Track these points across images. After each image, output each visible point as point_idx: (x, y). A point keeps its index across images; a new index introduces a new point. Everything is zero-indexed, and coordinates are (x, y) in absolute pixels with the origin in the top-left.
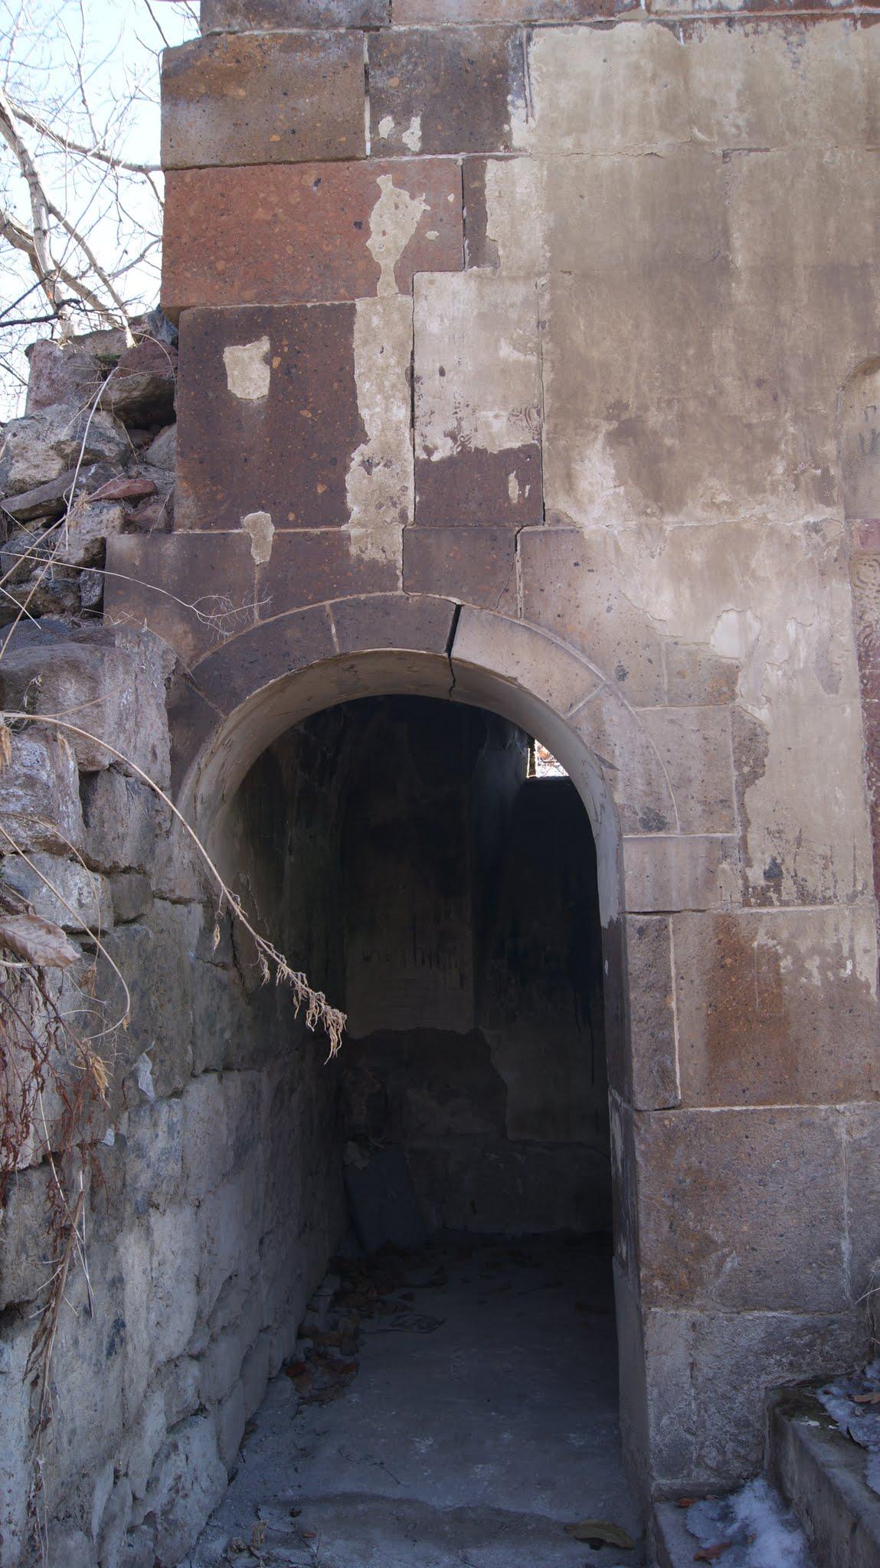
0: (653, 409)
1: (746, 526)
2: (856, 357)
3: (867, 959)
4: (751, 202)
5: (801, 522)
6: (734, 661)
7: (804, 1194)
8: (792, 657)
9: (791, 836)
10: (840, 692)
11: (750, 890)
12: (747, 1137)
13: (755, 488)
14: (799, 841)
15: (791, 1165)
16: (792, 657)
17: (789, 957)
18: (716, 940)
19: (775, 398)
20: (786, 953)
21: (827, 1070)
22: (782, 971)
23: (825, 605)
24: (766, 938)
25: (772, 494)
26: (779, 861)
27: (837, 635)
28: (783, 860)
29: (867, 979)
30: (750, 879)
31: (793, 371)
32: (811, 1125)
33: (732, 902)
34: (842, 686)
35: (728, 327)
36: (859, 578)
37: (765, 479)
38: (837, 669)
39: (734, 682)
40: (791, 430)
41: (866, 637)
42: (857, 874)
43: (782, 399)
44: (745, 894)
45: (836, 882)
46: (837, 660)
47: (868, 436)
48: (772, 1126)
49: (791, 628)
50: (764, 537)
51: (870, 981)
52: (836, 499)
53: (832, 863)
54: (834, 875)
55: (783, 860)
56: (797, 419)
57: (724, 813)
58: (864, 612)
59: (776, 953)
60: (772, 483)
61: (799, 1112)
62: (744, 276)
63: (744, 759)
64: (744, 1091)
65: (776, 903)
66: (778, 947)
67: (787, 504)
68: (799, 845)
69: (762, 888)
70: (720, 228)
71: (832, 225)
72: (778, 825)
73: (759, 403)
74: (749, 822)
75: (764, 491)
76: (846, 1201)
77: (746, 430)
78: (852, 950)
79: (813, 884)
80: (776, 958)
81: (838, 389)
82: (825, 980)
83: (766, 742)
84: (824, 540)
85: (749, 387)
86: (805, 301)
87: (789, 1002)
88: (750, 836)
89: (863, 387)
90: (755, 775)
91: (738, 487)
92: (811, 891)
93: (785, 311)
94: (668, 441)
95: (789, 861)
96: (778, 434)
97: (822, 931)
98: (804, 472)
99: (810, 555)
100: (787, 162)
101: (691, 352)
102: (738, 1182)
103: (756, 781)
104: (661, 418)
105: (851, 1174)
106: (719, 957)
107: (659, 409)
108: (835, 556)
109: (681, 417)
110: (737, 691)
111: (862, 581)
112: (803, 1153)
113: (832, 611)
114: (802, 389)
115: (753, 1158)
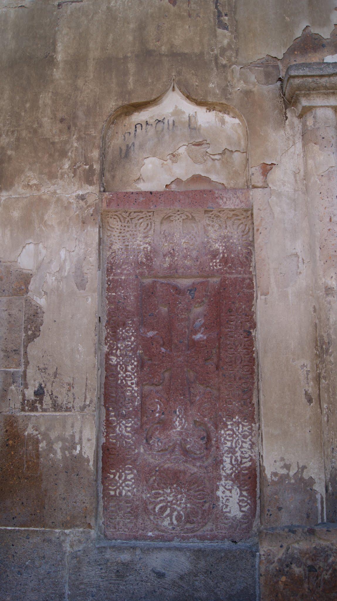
0: (4, 136)
1: (44, 197)
2: (115, 105)
3: (89, 444)
4: (70, 28)
5: (74, 194)
6: (30, 272)
7: (43, 581)
8: (61, 269)
9: (51, 371)
10: (87, 289)
11: (26, 402)
12: (13, 545)
13: (52, 176)
14: (55, 375)
15: (37, 563)
16: (61, 269)
17: (44, 442)
18: (5, 430)
19: (69, 128)
20: (43, 439)
21: (61, 509)
22: (40, 449)
23: (83, 240)
24: (32, 430)
25: (61, 179)
26: (43, 386)
27: (88, 257)
28: (45, 385)
29: (88, 456)
30: (26, 395)
31: (80, 114)
32: (50, 541)
33: (15, 408)
34: (88, 286)
35: (49, 92)
36: (109, 226)
37: (58, 172)
38: (86, 276)
39: (29, 284)
40: (75, 145)
41: (112, 258)
42: (87, 395)
43: (73, 128)
44: (23, 404)
45: (74, 398)
46: (85, 271)
47: (124, 148)
48: (27, 540)
49: (63, 253)
50: (53, 203)
51: (90, 457)
52: (95, 182)
53: (73, 387)
54: (73, 394)
55: (45, 385)
56: (79, 139)
57: (15, 357)
58: (112, 244)
59: (38, 439)
60: (62, 174)
61: (43, 533)
62: (61, 65)
63: (29, 327)
64: (13, 518)
65: (39, 410)
66: (39, 436)
67: (68, 185)
68: (55, 377)
69: (32, 401)
70: (51, 41)
71: (111, 36)
72: (44, 365)
73: (61, 131)
74: (28, 362)
75: (57, 178)
76: (67, 587)
77: (51, 146)
78: (81, 439)
79: (61, 400)
80: (38, 442)
81: (104, 122)
82: (64, 456)
83: (43, 317)
84: (86, 204)
85: (56, 123)
86: (92, 77)
87: (43, 468)
88: (28, 371)
89: (124, 123)
90: (35, 336)
91: (43, 176)
92: (60, 404)
93: (80, 82)
94: (9, 152)
95: (49, 385)
96: (68, 146)
97: (64, 427)
98: (79, 167)
99: (77, 213)
100: (91, 7)
101: (28, 105)
102: (6, 571)
103: (35, 339)
104: (7, 140)
105: (71, 571)
106: (6, 440)
107: (7, 135)
108: (92, 212)
109: (18, 139)
110: (29, 288)
111: (111, 227)
112: (44, 557)
113: (86, 244)
114: (84, 123)
115: (15, 558)
